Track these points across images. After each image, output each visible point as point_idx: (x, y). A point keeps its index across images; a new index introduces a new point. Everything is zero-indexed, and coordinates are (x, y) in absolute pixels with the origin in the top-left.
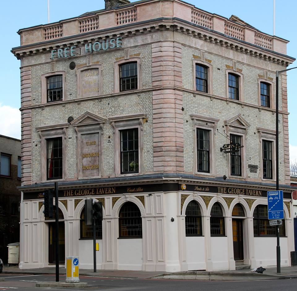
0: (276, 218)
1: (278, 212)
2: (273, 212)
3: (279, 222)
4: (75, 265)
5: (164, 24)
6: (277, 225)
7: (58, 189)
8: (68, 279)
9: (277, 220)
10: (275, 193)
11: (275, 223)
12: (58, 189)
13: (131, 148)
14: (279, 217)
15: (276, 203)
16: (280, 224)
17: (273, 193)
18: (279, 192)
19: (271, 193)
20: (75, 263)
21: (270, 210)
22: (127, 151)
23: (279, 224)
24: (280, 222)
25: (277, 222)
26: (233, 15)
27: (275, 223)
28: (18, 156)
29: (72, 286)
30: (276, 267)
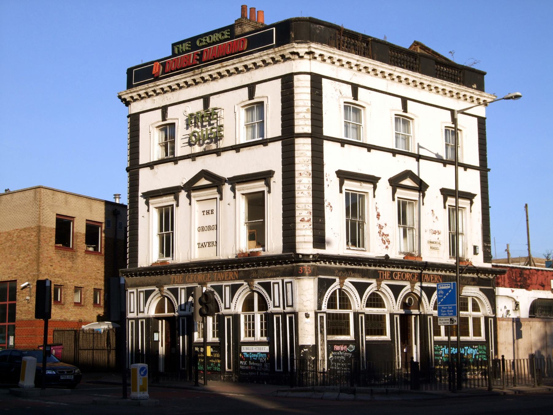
0: (449, 315)
1: (450, 306)
2: (444, 307)
3: (453, 321)
4: (142, 375)
5: (295, 51)
6: (449, 324)
7: (247, 221)
8: (133, 394)
9: (449, 318)
10: (446, 286)
11: (447, 321)
12: (247, 221)
13: (167, 229)
14: (452, 314)
15: (448, 295)
16: (454, 324)
17: (444, 286)
18: (451, 284)
19: (441, 286)
20: (142, 373)
21: (440, 304)
22: (169, 232)
23: (453, 323)
24: (454, 321)
25: (449, 321)
26: (417, 40)
27: (447, 321)
28: (57, 214)
29: (137, 402)
30: (211, 149)
